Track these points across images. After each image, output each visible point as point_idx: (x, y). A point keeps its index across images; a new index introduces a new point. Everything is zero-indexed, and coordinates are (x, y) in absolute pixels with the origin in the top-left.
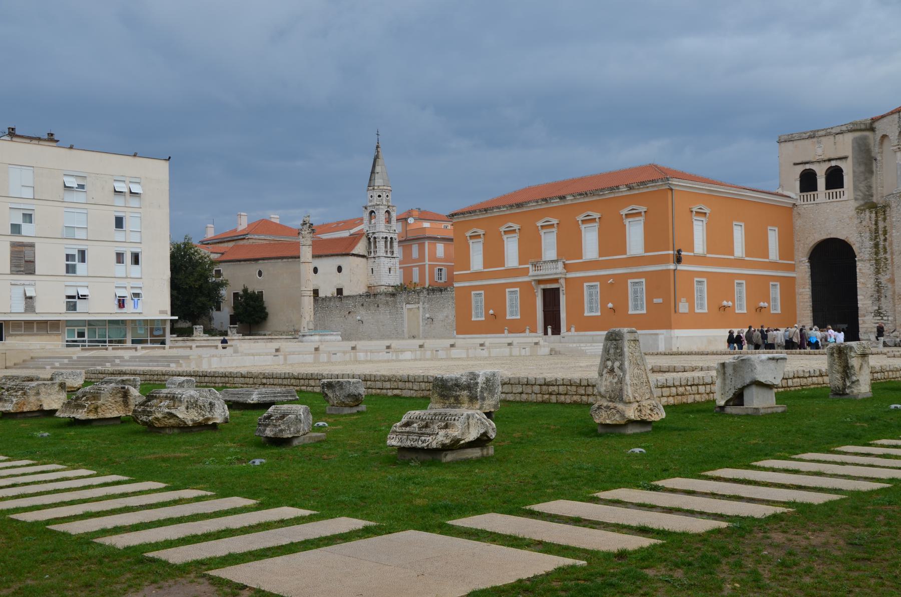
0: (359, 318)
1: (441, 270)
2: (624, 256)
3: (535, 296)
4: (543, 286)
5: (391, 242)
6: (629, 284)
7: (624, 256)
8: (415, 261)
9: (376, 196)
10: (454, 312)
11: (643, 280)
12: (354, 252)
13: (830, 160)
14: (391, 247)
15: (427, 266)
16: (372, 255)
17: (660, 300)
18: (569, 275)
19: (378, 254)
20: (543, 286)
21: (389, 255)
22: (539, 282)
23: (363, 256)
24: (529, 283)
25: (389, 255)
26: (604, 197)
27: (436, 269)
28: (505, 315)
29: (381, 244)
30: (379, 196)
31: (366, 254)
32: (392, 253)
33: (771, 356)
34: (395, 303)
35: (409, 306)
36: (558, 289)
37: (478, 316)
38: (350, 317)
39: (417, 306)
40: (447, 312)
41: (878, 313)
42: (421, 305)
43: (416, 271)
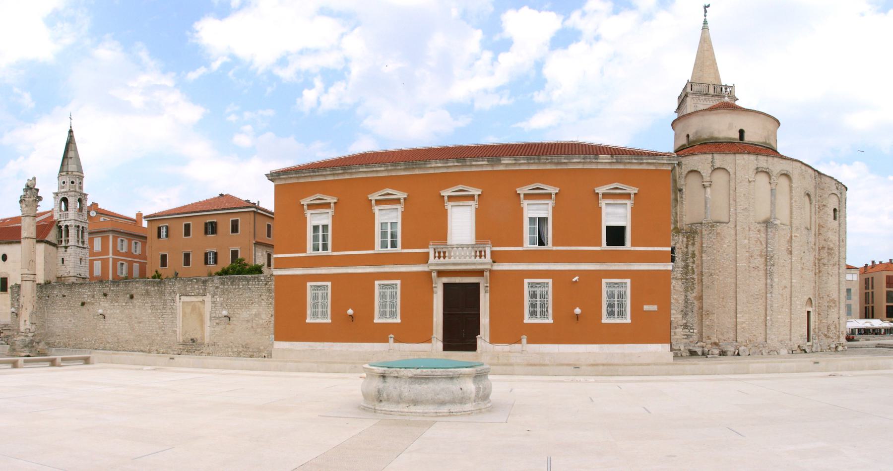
0: (101, 311)
1: (122, 264)
2: (598, 248)
3: (431, 291)
4: (446, 280)
5: (83, 232)
6: (377, 287)
7: (598, 248)
8: (98, 254)
9: (68, 184)
10: (272, 310)
11: (329, 284)
12: (47, 239)
13: (735, 174)
14: (82, 237)
15: (111, 261)
16: (63, 244)
17: (654, 308)
18: (498, 267)
19: (70, 243)
20: (446, 280)
21: (81, 245)
22: (441, 273)
23: (54, 245)
24: (430, 273)
25: (81, 245)
26: (628, 167)
27: (119, 263)
28: (373, 318)
29: (72, 232)
30: (73, 182)
31: (56, 242)
32: (83, 242)
33: (482, 367)
34: (162, 293)
35: (184, 299)
36: (477, 285)
37: (318, 309)
38: (84, 310)
39: (200, 299)
40: (255, 308)
41: (686, 326)
42: (208, 298)
43: (98, 265)
